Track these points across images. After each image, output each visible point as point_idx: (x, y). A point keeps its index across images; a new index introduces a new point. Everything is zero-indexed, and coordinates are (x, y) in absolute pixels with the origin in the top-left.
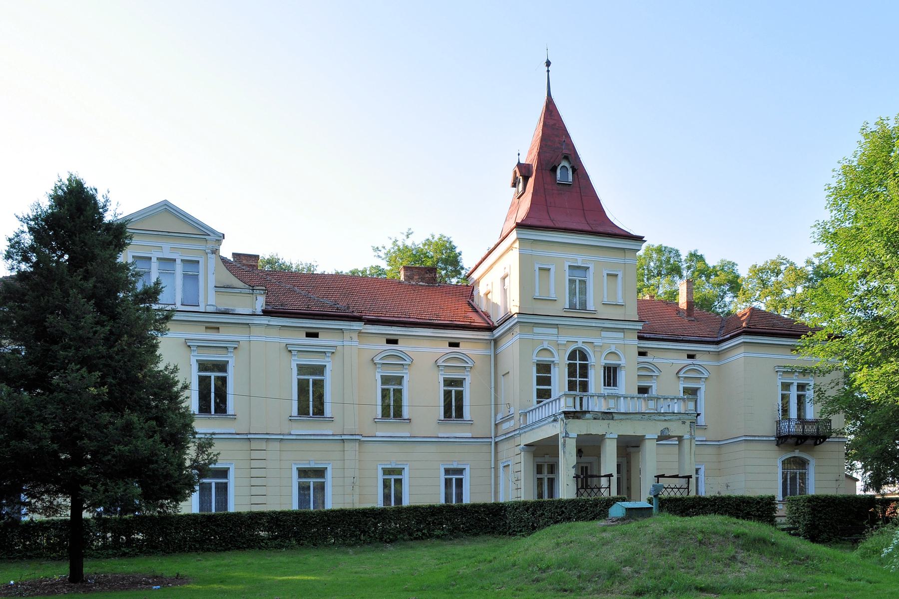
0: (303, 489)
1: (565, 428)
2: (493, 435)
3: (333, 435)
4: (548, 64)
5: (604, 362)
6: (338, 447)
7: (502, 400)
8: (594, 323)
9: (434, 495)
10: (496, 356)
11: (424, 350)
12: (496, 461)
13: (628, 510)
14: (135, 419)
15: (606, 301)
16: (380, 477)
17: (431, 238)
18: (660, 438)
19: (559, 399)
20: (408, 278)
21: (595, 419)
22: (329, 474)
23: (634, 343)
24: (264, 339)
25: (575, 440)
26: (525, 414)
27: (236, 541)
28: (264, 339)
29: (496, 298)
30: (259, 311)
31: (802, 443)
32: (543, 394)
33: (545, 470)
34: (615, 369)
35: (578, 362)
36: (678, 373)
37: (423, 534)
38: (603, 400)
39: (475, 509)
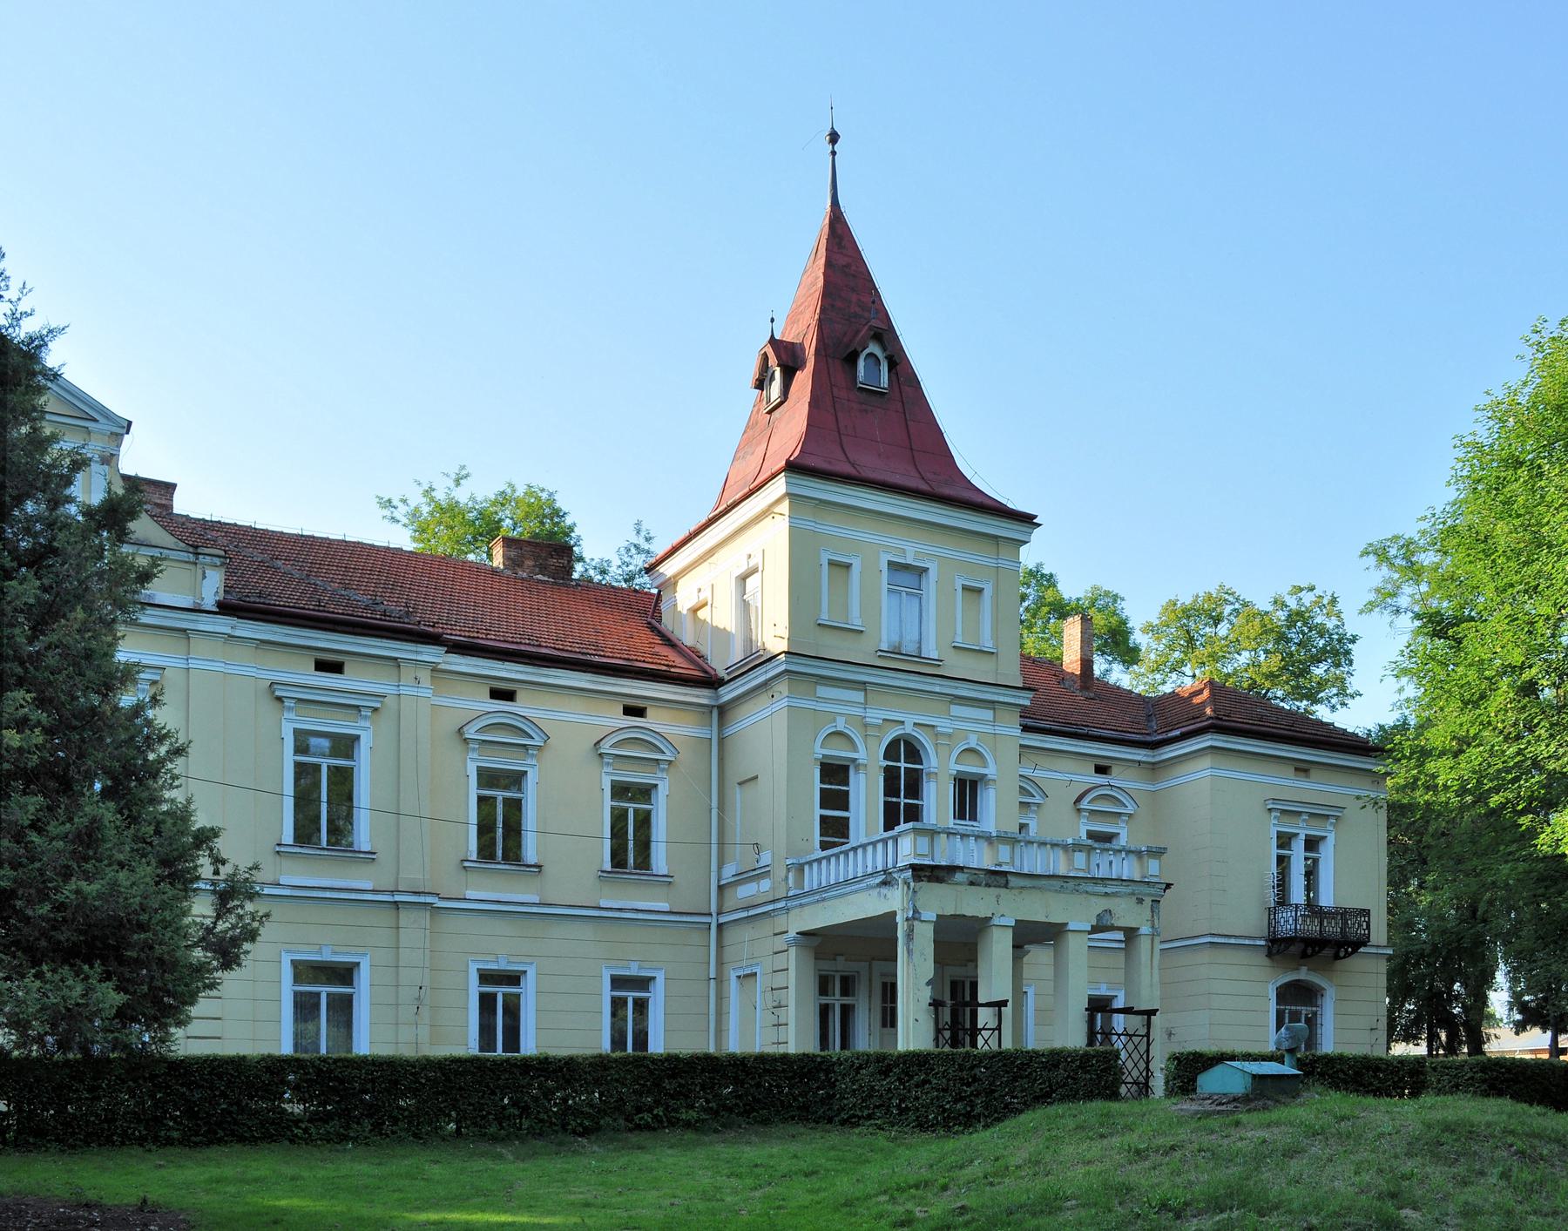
0: (305, 1008)
2: (714, 909)
3: (374, 891)
4: (834, 138)
6: (385, 917)
8: (937, 686)
9: (590, 1036)
10: (722, 741)
11: (571, 718)
13: (1258, 1079)
14: (109, 816)
15: (959, 640)
16: (474, 989)
17: (509, 491)
18: (1095, 929)
20: (513, 562)
21: (972, 884)
22: (364, 977)
23: (1011, 729)
24: (219, 667)
25: (931, 927)
26: (800, 868)
27: (236, 1122)
28: (219, 667)
29: (723, 616)
30: (209, 602)
31: (1314, 954)
32: (834, 830)
35: (903, 765)
37: (656, 1117)
38: (985, 844)
39: (675, 1066)
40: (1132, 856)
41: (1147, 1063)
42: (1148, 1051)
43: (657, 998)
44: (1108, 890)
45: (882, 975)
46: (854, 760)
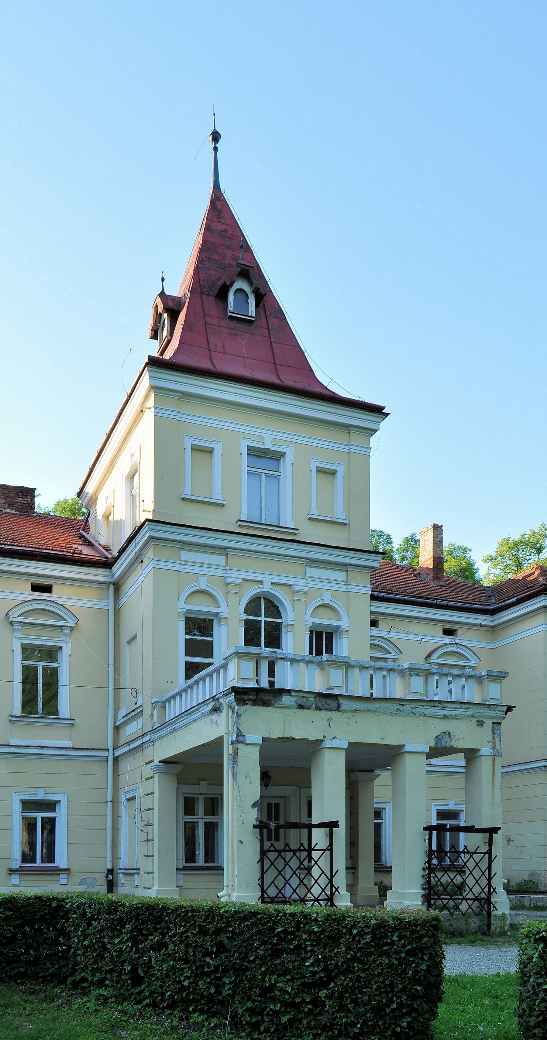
1: (237, 723)
2: (110, 745)
4: (216, 137)
5: (310, 620)
7: (126, 682)
10: (117, 612)
12: (116, 788)
15: (314, 513)
18: (437, 751)
19: (225, 667)
21: (301, 707)
26: (162, 705)
33: (200, 808)
34: (330, 636)
35: (263, 619)
36: (429, 656)
40: (471, 681)
41: (490, 879)
42: (490, 868)
43: (62, 817)
44: (447, 713)
45: (183, 794)
46: (217, 615)
